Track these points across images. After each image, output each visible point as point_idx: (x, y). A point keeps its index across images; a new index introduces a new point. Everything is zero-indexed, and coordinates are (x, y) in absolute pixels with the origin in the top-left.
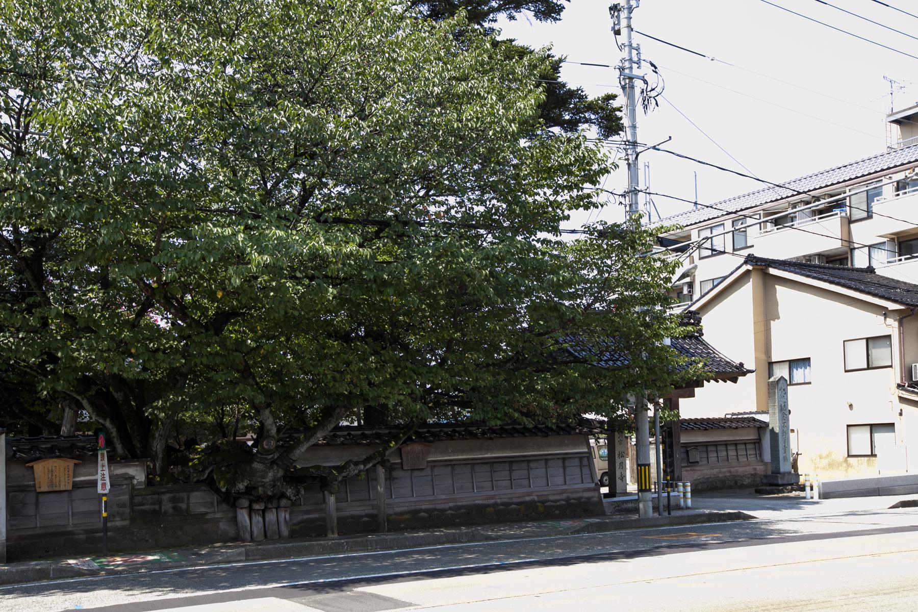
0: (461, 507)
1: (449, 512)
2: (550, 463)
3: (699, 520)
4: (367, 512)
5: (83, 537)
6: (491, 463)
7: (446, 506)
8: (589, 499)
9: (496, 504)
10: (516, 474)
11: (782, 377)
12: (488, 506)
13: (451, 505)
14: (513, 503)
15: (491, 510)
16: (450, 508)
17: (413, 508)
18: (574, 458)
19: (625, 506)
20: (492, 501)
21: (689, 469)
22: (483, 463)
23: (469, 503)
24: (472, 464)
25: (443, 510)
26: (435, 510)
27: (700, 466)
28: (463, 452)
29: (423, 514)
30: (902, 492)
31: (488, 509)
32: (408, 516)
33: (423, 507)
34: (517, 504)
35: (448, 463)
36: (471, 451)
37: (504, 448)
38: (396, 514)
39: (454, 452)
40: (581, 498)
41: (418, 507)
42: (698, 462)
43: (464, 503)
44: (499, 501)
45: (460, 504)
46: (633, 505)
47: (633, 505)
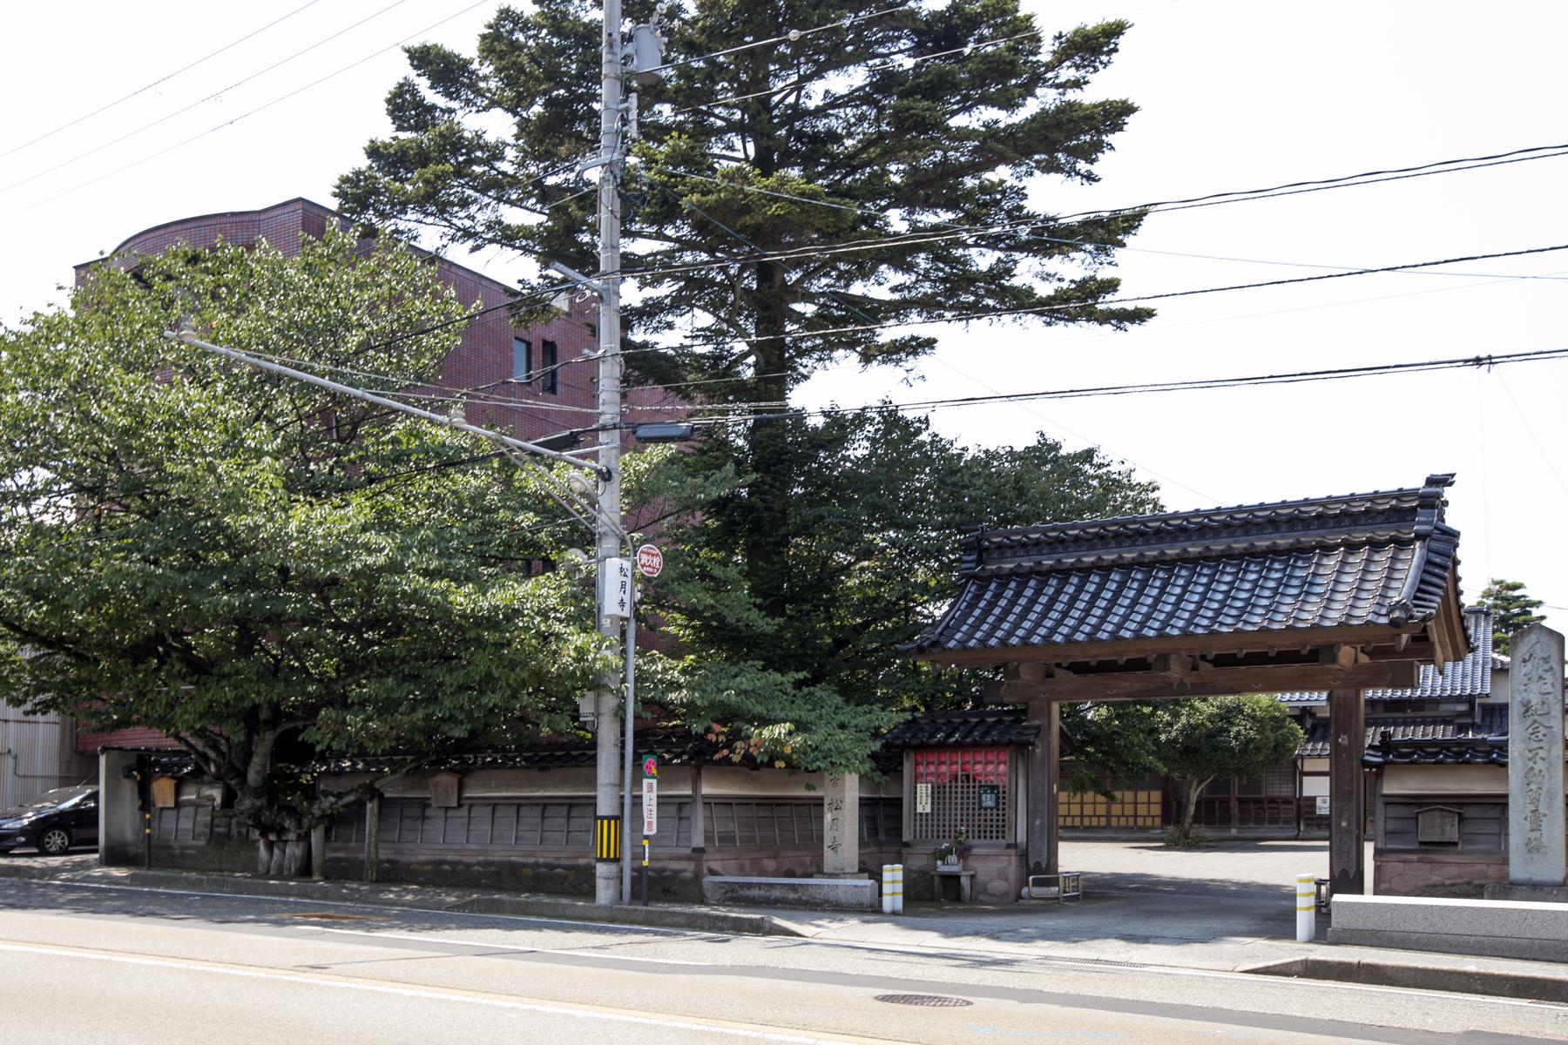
0: (492, 863)
1: (476, 868)
2: (524, 811)
3: (669, 920)
4: (390, 856)
5: (178, 852)
6: (544, 805)
7: (475, 860)
8: (677, 872)
9: (536, 865)
10: (575, 823)
11: (1169, 669)
12: (525, 865)
13: (481, 858)
14: (559, 866)
15: (528, 871)
16: (478, 864)
17: (437, 858)
18: (669, 804)
19: (746, 892)
20: (531, 860)
21: (1414, 857)
22: (532, 805)
23: (502, 859)
24: (519, 805)
25: (469, 865)
26: (460, 863)
27: (1463, 853)
28: (508, 787)
29: (446, 867)
30: (1353, 941)
31: (524, 870)
32: (429, 868)
33: (449, 858)
34: (564, 867)
35: (487, 802)
36: (519, 786)
37: (562, 784)
38: (417, 863)
39: (498, 787)
40: (664, 870)
41: (442, 857)
42: (1455, 844)
43: (497, 859)
44: (541, 860)
45: (492, 858)
46: (762, 892)
47: (762, 892)
